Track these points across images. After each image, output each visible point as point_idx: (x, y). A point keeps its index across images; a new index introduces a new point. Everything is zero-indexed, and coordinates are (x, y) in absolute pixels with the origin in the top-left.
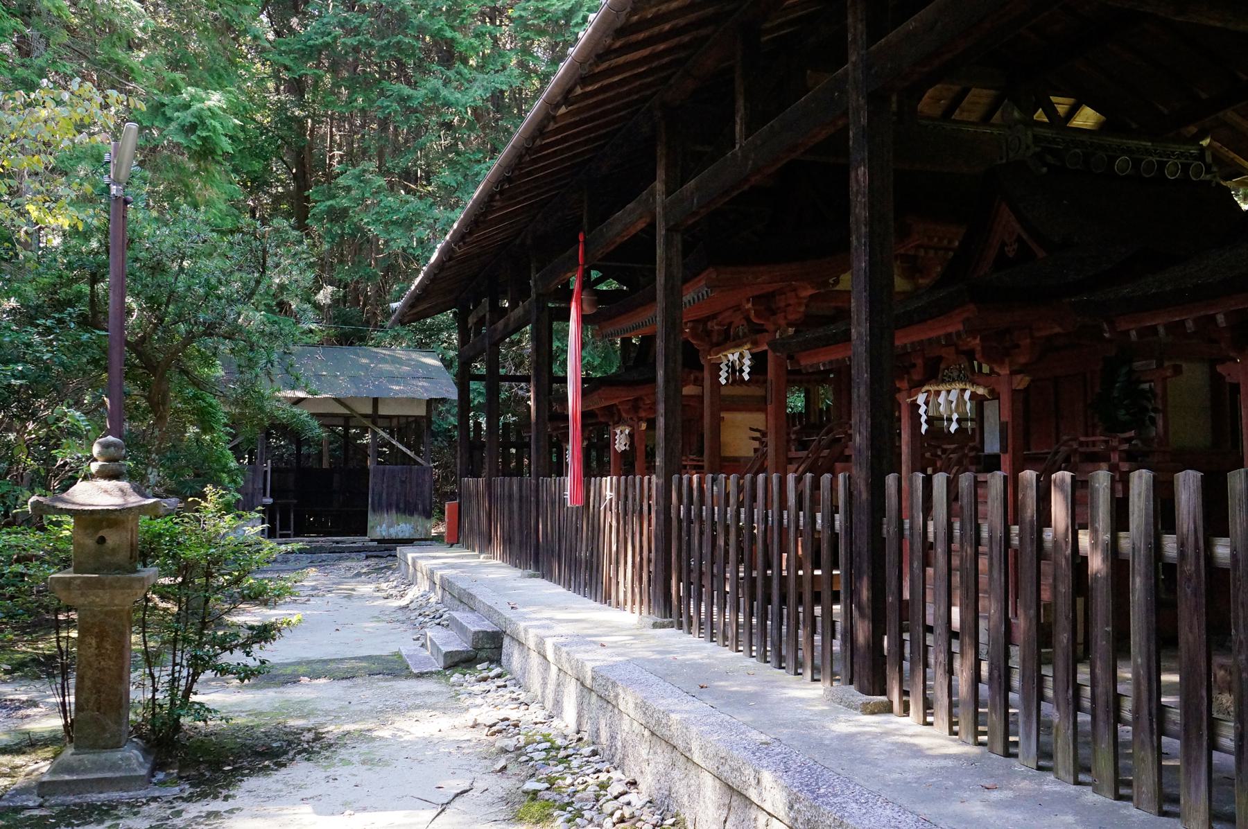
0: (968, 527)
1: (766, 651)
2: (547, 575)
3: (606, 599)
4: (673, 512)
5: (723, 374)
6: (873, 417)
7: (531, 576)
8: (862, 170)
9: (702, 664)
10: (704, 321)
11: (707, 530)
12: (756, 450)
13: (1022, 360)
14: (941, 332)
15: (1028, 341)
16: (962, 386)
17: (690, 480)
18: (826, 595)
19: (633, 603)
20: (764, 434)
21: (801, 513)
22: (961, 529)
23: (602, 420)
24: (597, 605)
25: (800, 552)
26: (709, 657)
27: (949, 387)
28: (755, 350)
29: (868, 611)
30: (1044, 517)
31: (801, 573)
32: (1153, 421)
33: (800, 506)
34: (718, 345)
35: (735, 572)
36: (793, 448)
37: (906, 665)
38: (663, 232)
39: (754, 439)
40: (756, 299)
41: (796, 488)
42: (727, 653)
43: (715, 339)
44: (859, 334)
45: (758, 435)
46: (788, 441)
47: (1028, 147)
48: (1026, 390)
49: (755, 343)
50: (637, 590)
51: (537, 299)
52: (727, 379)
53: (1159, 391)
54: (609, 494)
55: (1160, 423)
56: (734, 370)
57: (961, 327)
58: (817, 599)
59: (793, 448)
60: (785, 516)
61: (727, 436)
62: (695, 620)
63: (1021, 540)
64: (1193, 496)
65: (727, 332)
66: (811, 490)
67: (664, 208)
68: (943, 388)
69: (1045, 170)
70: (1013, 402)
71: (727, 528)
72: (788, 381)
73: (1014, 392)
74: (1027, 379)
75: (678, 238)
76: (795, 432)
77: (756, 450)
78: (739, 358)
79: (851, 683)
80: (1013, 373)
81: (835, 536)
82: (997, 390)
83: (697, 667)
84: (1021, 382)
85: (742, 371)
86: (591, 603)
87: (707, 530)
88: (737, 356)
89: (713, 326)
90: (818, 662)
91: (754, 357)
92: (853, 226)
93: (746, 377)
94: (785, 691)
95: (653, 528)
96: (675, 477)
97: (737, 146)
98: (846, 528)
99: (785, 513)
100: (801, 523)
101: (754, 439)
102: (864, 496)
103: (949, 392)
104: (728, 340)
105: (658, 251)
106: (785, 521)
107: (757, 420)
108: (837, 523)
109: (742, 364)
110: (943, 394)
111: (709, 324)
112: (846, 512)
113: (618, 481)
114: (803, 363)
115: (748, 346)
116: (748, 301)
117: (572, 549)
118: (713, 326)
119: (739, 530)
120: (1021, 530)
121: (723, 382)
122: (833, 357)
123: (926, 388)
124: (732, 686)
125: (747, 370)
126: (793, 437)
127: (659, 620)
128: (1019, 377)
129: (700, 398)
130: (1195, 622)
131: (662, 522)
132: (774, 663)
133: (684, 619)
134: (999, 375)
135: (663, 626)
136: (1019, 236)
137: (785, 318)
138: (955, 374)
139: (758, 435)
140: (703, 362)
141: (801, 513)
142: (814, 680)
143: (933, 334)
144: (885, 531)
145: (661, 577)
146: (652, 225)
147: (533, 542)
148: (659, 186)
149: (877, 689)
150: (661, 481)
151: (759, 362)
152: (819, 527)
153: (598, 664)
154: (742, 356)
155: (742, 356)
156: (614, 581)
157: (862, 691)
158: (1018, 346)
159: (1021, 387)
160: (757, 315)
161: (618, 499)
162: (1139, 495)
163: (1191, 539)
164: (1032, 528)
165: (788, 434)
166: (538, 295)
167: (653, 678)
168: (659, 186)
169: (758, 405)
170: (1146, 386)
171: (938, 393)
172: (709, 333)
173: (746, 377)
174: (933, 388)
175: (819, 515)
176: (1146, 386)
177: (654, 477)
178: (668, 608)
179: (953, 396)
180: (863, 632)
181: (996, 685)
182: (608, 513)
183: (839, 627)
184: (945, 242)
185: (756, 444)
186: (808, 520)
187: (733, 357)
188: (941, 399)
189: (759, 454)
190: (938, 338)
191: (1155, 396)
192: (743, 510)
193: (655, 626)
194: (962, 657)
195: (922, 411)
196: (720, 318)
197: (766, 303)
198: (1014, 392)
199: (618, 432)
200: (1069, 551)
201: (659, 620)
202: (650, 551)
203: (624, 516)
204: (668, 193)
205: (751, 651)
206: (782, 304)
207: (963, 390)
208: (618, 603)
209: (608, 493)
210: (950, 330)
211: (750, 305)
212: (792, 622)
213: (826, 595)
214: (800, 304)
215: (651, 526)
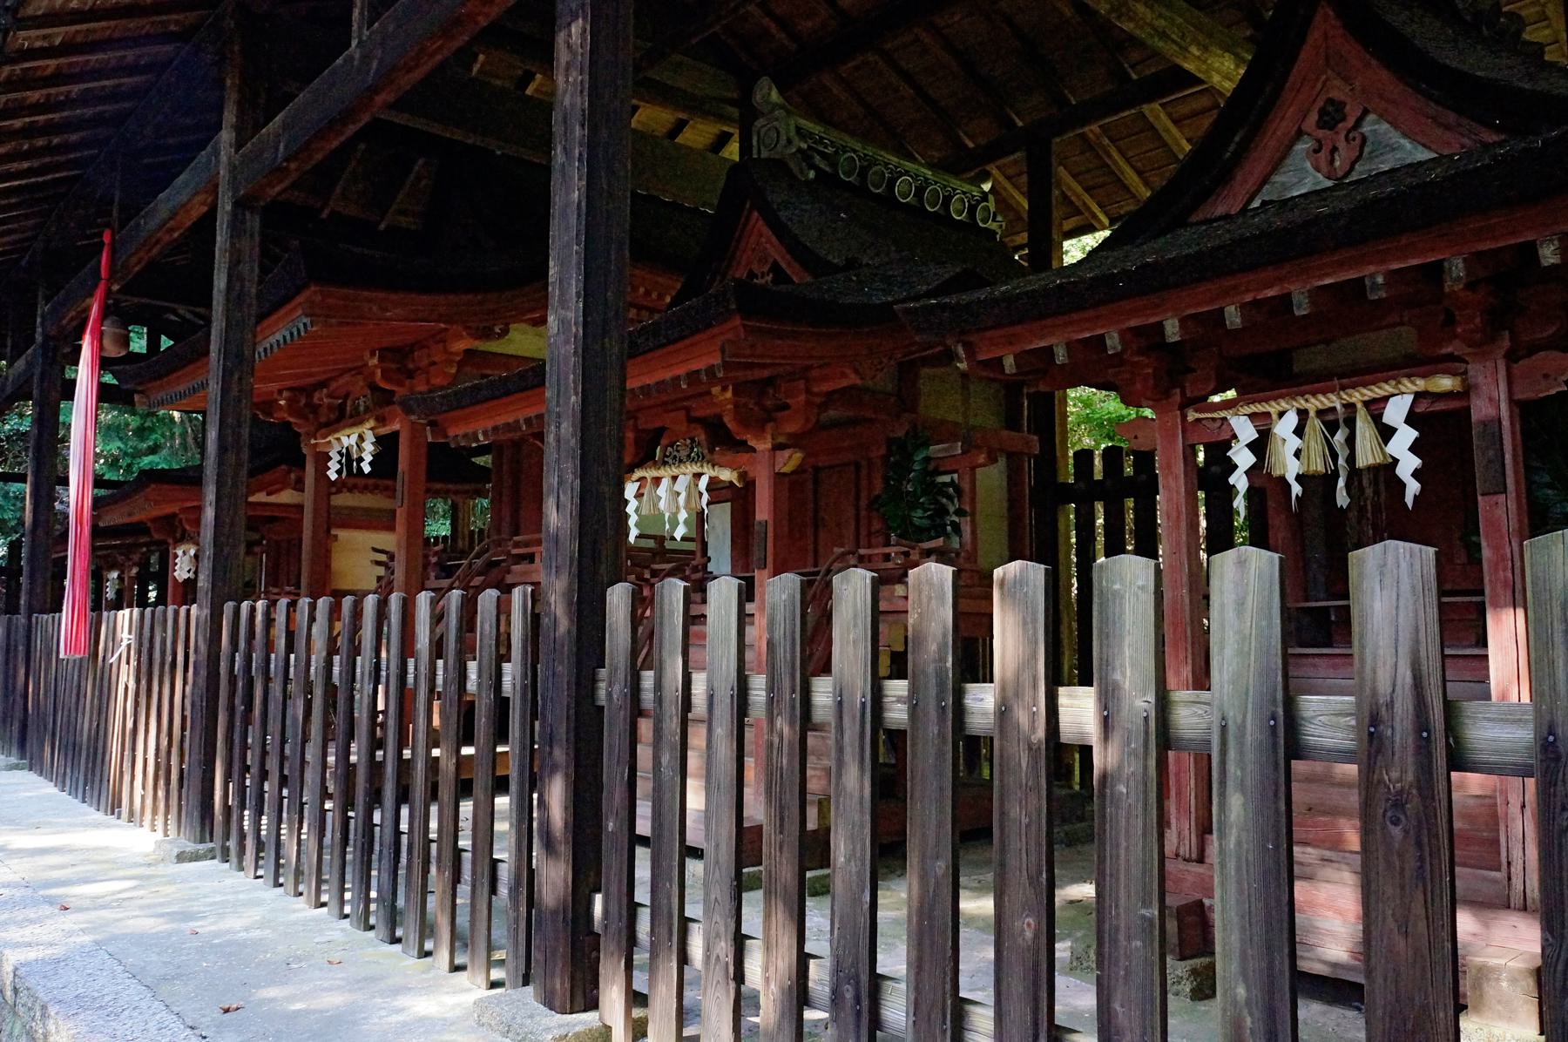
0: (786, 683)
1: (368, 901)
2: (35, 764)
3: (114, 807)
4: (223, 666)
5: (333, 466)
6: (584, 475)
7: (16, 767)
8: (575, 29)
9: (243, 945)
10: (308, 391)
11: (276, 688)
12: (379, 579)
13: (791, 428)
14: (681, 371)
15: (802, 397)
16: (696, 469)
17: (253, 610)
18: (481, 782)
19: (155, 812)
20: (392, 557)
21: (440, 663)
22: (771, 688)
23: (156, 536)
24: (99, 816)
25: (436, 721)
26: (261, 925)
27: (675, 471)
28: (383, 431)
29: (564, 850)
30: (973, 659)
31: (436, 752)
32: (957, 528)
33: (438, 649)
34: (328, 425)
35: (321, 760)
36: (433, 574)
37: (641, 957)
38: (228, 208)
39: (378, 563)
40: (386, 353)
41: (432, 631)
42: (301, 908)
43: (323, 419)
44: (563, 322)
45: (383, 558)
46: (425, 566)
47: (789, 142)
48: (797, 472)
49: (381, 420)
50: (161, 794)
51: (44, 345)
52: (339, 472)
53: (966, 486)
54: (126, 636)
55: (966, 529)
56: (348, 458)
57: (717, 361)
58: (464, 788)
59: (433, 574)
60: (411, 668)
61: (339, 562)
62: (250, 843)
63: (914, 710)
64: (1407, 601)
65: (342, 407)
66: (460, 629)
67: (233, 169)
68: (665, 473)
69: (812, 174)
70: (776, 485)
71: (308, 688)
72: (428, 491)
73: (779, 477)
74: (798, 456)
75: (254, 222)
76: (436, 553)
77: (379, 579)
78: (357, 442)
79: (526, 981)
80: (778, 447)
81: (502, 705)
82: (751, 475)
83: (234, 951)
84: (790, 461)
85: (361, 460)
86: (90, 813)
87: (276, 688)
88: (354, 438)
89: (321, 397)
90: (463, 920)
91: (379, 440)
92: (557, 129)
93: (367, 469)
94: (401, 1001)
95: (188, 689)
96: (229, 607)
97: (354, 43)
98: (524, 687)
99: (411, 663)
100: (440, 680)
101: (378, 563)
102: (564, 625)
103: (675, 478)
104: (343, 417)
105: (218, 238)
106: (410, 678)
107: (387, 540)
108: (507, 681)
109: (360, 449)
110: (665, 483)
111: (317, 395)
112: (524, 658)
113: (142, 615)
114: (451, 433)
115: (371, 423)
116: (373, 354)
117: (72, 726)
118: (321, 397)
119: (330, 690)
120: (913, 690)
121: (333, 476)
122: (501, 420)
123: (638, 474)
124: (292, 998)
125: (368, 458)
126: (434, 560)
127: (191, 847)
128: (786, 453)
129: (299, 508)
130: (1418, 909)
131: (202, 682)
132: (382, 930)
133: (232, 844)
134: (754, 450)
135: (195, 857)
136: (775, 263)
137: (428, 382)
138: (683, 453)
139: (383, 558)
140: (305, 451)
141: (440, 663)
142: (456, 968)
143: (668, 375)
144: (602, 693)
145: (197, 775)
146: (211, 215)
147: (18, 714)
148: (226, 136)
149: (579, 1000)
150: (206, 611)
151: (386, 445)
152: (472, 686)
153: (32, 955)
154: (361, 438)
155: (361, 438)
156: (127, 778)
157: (549, 1002)
158: (786, 407)
159: (787, 469)
160: (386, 375)
161: (140, 645)
162: (1240, 604)
163: (1404, 707)
164: (941, 684)
165: (426, 557)
166: (46, 337)
167: (134, 990)
168: (226, 136)
169: (383, 521)
170: (946, 479)
171: (657, 481)
172: (315, 409)
173: (367, 469)
174: (649, 473)
175: (472, 667)
176: (946, 479)
177: (194, 608)
178: (209, 823)
179: (682, 485)
180: (554, 877)
181: (848, 1015)
182: (124, 666)
183: (504, 872)
184: (654, 296)
185: (381, 571)
186: (453, 674)
187: (348, 439)
188: (662, 491)
189: (383, 583)
190: (677, 379)
191: (959, 491)
192: (337, 659)
193: (181, 858)
194: (768, 949)
195: (630, 509)
196: (334, 385)
197: (399, 357)
198: (779, 477)
199: (180, 552)
200: (1041, 733)
201: (191, 847)
202: (183, 729)
203: (145, 673)
204: (239, 145)
205: (342, 902)
206: (425, 362)
207: (698, 476)
208: (131, 813)
209: (125, 635)
210: (694, 366)
211: (375, 361)
212: (417, 862)
213: (481, 782)
214: (449, 362)
215: (182, 690)
